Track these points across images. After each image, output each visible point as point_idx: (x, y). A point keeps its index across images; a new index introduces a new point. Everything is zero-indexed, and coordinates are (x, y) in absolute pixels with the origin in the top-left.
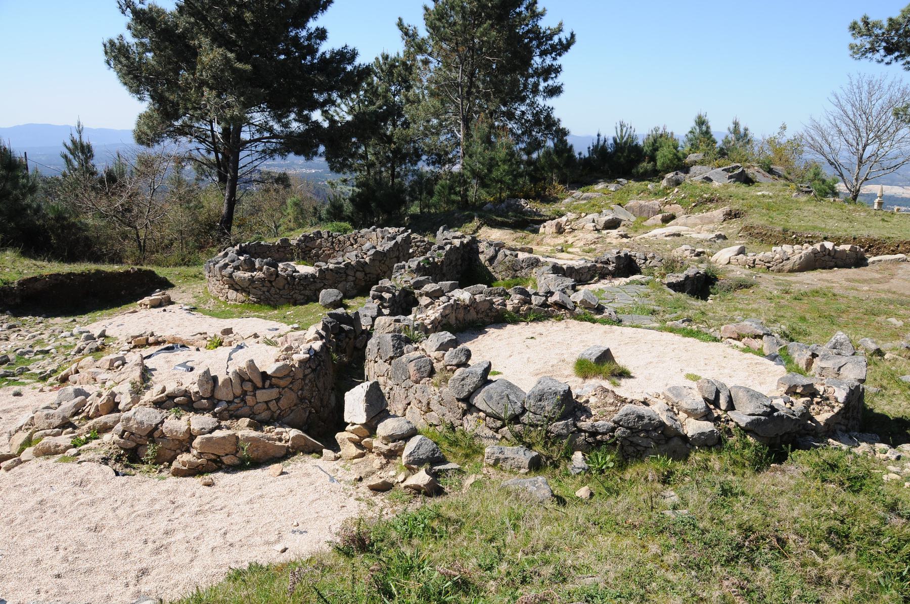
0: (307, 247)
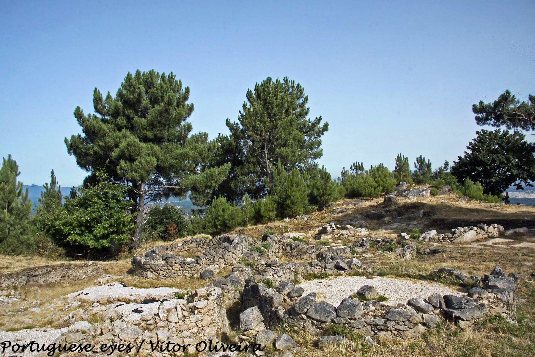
0: (188, 247)
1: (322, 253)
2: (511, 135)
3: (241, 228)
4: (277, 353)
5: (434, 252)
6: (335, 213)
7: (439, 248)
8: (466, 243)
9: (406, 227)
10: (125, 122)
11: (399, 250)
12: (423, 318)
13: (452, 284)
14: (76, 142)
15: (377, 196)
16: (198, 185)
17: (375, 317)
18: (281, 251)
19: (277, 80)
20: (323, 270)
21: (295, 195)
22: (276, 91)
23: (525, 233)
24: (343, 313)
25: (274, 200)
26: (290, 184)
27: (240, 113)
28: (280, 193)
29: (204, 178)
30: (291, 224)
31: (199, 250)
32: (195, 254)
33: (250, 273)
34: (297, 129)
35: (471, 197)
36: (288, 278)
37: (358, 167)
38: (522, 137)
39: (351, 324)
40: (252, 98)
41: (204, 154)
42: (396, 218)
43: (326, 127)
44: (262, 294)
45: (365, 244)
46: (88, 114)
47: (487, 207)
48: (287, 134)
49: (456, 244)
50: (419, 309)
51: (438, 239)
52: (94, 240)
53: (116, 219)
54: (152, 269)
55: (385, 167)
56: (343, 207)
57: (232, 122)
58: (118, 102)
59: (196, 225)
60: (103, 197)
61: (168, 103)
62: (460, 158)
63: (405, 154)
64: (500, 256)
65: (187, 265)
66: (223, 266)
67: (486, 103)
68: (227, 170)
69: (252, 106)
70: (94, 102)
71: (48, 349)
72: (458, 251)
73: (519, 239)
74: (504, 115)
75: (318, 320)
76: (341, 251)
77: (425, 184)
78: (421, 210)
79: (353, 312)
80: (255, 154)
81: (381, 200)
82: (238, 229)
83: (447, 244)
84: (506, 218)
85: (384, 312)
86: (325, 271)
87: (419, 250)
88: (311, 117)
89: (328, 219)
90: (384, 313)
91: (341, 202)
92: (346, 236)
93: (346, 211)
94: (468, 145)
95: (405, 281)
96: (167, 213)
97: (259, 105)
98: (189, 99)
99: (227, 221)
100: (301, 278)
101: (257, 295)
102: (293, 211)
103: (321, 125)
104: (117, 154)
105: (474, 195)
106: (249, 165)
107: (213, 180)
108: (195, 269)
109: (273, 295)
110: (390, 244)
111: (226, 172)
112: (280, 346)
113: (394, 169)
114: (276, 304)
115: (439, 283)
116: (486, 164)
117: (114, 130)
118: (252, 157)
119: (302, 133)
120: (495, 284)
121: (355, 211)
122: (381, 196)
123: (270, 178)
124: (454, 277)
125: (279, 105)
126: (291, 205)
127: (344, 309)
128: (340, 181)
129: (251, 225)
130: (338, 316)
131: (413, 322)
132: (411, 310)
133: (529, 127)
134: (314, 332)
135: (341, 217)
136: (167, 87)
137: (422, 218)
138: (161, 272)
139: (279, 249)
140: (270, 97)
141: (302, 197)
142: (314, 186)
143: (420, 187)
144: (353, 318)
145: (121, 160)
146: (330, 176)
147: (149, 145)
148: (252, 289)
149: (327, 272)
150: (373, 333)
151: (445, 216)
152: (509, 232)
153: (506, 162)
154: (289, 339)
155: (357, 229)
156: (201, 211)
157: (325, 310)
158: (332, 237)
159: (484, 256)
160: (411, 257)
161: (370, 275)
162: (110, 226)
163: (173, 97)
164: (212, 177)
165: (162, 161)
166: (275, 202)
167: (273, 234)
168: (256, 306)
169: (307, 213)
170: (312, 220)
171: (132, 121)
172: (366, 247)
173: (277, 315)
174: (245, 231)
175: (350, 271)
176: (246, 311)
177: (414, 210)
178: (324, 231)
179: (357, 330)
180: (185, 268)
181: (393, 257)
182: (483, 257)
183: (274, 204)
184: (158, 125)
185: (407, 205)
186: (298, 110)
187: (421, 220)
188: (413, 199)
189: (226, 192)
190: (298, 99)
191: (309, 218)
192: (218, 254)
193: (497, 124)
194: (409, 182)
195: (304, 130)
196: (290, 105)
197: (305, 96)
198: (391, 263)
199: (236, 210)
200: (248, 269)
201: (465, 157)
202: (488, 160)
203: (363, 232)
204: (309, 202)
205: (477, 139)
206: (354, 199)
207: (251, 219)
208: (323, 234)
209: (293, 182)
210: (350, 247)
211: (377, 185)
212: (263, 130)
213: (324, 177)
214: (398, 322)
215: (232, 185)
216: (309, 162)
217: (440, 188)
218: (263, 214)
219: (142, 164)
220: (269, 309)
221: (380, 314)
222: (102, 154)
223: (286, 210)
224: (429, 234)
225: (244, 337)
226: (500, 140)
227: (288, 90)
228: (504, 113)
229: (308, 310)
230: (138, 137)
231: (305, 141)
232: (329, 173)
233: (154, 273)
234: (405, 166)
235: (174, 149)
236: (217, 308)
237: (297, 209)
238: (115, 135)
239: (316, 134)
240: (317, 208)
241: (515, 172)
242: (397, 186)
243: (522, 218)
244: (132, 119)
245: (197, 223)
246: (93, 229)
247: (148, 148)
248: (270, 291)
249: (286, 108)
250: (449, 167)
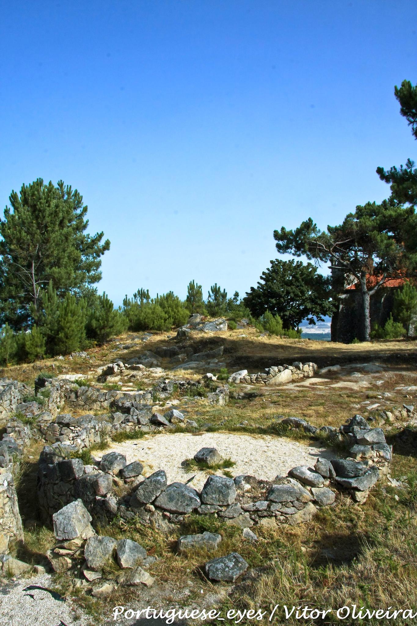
1: (118, 401)
2: (304, 267)
4: (122, 573)
5: (250, 396)
6: (118, 349)
7: (255, 391)
8: (280, 385)
9: (207, 366)
11: (211, 395)
12: (312, 493)
13: (300, 438)
15: (167, 330)
17: (254, 499)
18: (63, 400)
19: (50, 183)
20: (137, 427)
21: (70, 327)
22: (48, 196)
23: (339, 371)
24: (212, 499)
25: (44, 332)
26: (63, 312)
28: (50, 323)
30: (66, 363)
33: (29, 433)
34: (73, 245)
35: (272, 332)
36: (92, 441)
37: (143, 294)
38: (315, 269)
39: (222, 514)
40: (17, 202)
42: (192, 355)
43: (107, 246)
44: (79, 475)
45: (168, 389)
47: (291, 343)
48: (61, 251)
49: (271, 385)
50: (305, 482)
51: (251, 380)
55: (175, 295)
56: (128, 341)
62: (252, 289)
63: (198, 282)
64: (325, 398)
67: (288, 230)
69: (17, 213)
72: (278, 394)
73: (336, 378)
74: (306, 245)
75: (173, 511)
76: (140, 397)
77: (220, 316)
78: (221, 346)
79: (226, 496)
80: (19, 273)
81: (175, 334)
83: (261, 386)
84: (315, 355)
85: (264, 491)
86: (139, 428)
87: (233, 394)
88: (90, 232)
89: (110, 357)
90: (265, 493)
91: (124, 336)
92: (138, 377)
93: (132, 347)
94: (262, 275)
95: (242, 437)
97: (26, 212)
100: (109, 440)
101: (70, 477)
102: (66, 346)
103: (102, 243)
105: (274, 329)
106: (11, 288)
109: (96, 476)
110: (197, 387)
112: (126, 561)
113: (185, 298)
114: (103, 491)
115: (285, 438)
116: (280, 296)
118: (15, 278)
119: (79, 251)
120: (364, 437)
121: (143, 347)
122: (171, 329)
123: (37, 305)
124: (302, 429)
125: (52, 214)
126: (65, 339)
127: (212, 493)
128: (121, 311)
129: (13, 365)
130: (202, 503)
131: (303, 501)
132: (295, 484)
133: (327, 259)
134: (166, 529)
135: (127, 354)
137: (222, 355)
139: (61, 398)
140: (41, 203)
141: (78, 329)
142: (92, 316)
143: (216, 319)
144: (225, 504)
146: (113, 305)
148: (59, 468)
149: (141, 429)
150: (252, 522)
151: (249, 353)
152: (324, 371)
153: (300, 295)
154: (136, 547)
155: (151, 369)
157: (184, 496)
158: (121, 379)
159: (309, 399)
160: (224, 402)
161: (197, 431)
166: (45, 335)
167: (51, 377)
168: (79, 500)
169: (84, 349)
170: (91, 358)
172: (169, 392)
173: (106, 507)
174: (6, 372)
175: (171, 427)
176: (64, 508)
177: (212, 346)
178: (110, 372)
179: (231, 520)
181: (207, 404)
182: (307, 400)
183: (43, 337)
185: (204, 340)
186: (75, 223)
187: (222, 358)
188: (210, 334)
190: (75, 208)
191: (88, 355)
193: (298, 253)
194: (202, 314)
195: (81, 247)
196: (66, 215)
197: (84, 205)
198: (208, 412)
200: (28, 428)
201: (258, 287)
202: (283, 292)
203: (159, 372)
204: (86, 335)
205: (270, 269)
206: (140, 333)
207: (12, 356)
208: (108, 375)
209: (67, 310)
210: (150, 393)
211: (167, 317)
212: (31, 244)
213: (105, 305)
214: (284, 504)
216: (86, 287)
217: (238, 321)
218: (29, 351)
220: (91, 497)
221: (260, 495)
223: (59, 345)
224: (240, 374)
225: (62, 551)
226: (294, 271)
227: (63, 196)
228: (305, 242)
229: (157, 497)
231: (82, 261)
232: (111, 301)
234: (198, 295)
236: (9, 503)
237: (72, 345)
239: (95, 253)
240: (96, 342)
241: (309, 305)
242: (190, 318)
243: (331, 355)
248: (90, 469)
249: (61, 219)
250: (239, 298)
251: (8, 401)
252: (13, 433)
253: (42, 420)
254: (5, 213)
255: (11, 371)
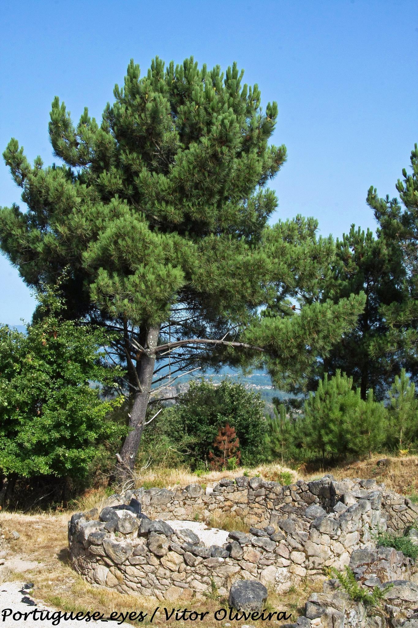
0: (227, 500)
3: (383, 457)
10: (120, 182)
14: (6, 224)
16: (280, 343)
27: (405, 174)
29: (296, 327)
31: (256, 510)
32: (242, 519)
41: (301, 268)
46: (36, 158)
52: (17, 455)
53: (71, 410)
54: (108, 556)
57: (381, 196)
58: (104, 133)
59: (280, 437)
60: (51, 354)
61: (221, 138)
65: (199, 559)
66: (301, 571)
68: (356, 311)
70: (51, 131)
71: (53, 617)
82: (374, 458)
96: (216, 401)
98: (275, 133)
99: (349, 436)
104: (93, 255)
107: (318, 332)
108: (221, 571)
111: (352, 314)
117: (95, 200)
129: (411, 453)
136: (222, 101)
138: (130, 570)
145: (101, 269)
147: (171, 239)
156: (295, 404)
162: (57, 426)
163: (231, 123)
164: (316, 324)
165: (200, 280)
171: (135, 178)
180: (193, 566)
184: (195, 192)
189: (357, 365)
192: (289, 538)
199: (373, 411)
215: (371, 348)
219: (146, 282)
222: (63, 253)
230: (148, 217)
233: (112, 568)
235: (231, 253)
238: (94, 210)
244: (137, 174)
245: (283, 432)
246: (17, 428)
247: (166, 247)
251: (356, 533)
252: (318, 620)
253: (398, 598)
254: (412, 158)
255: (402, 464)
